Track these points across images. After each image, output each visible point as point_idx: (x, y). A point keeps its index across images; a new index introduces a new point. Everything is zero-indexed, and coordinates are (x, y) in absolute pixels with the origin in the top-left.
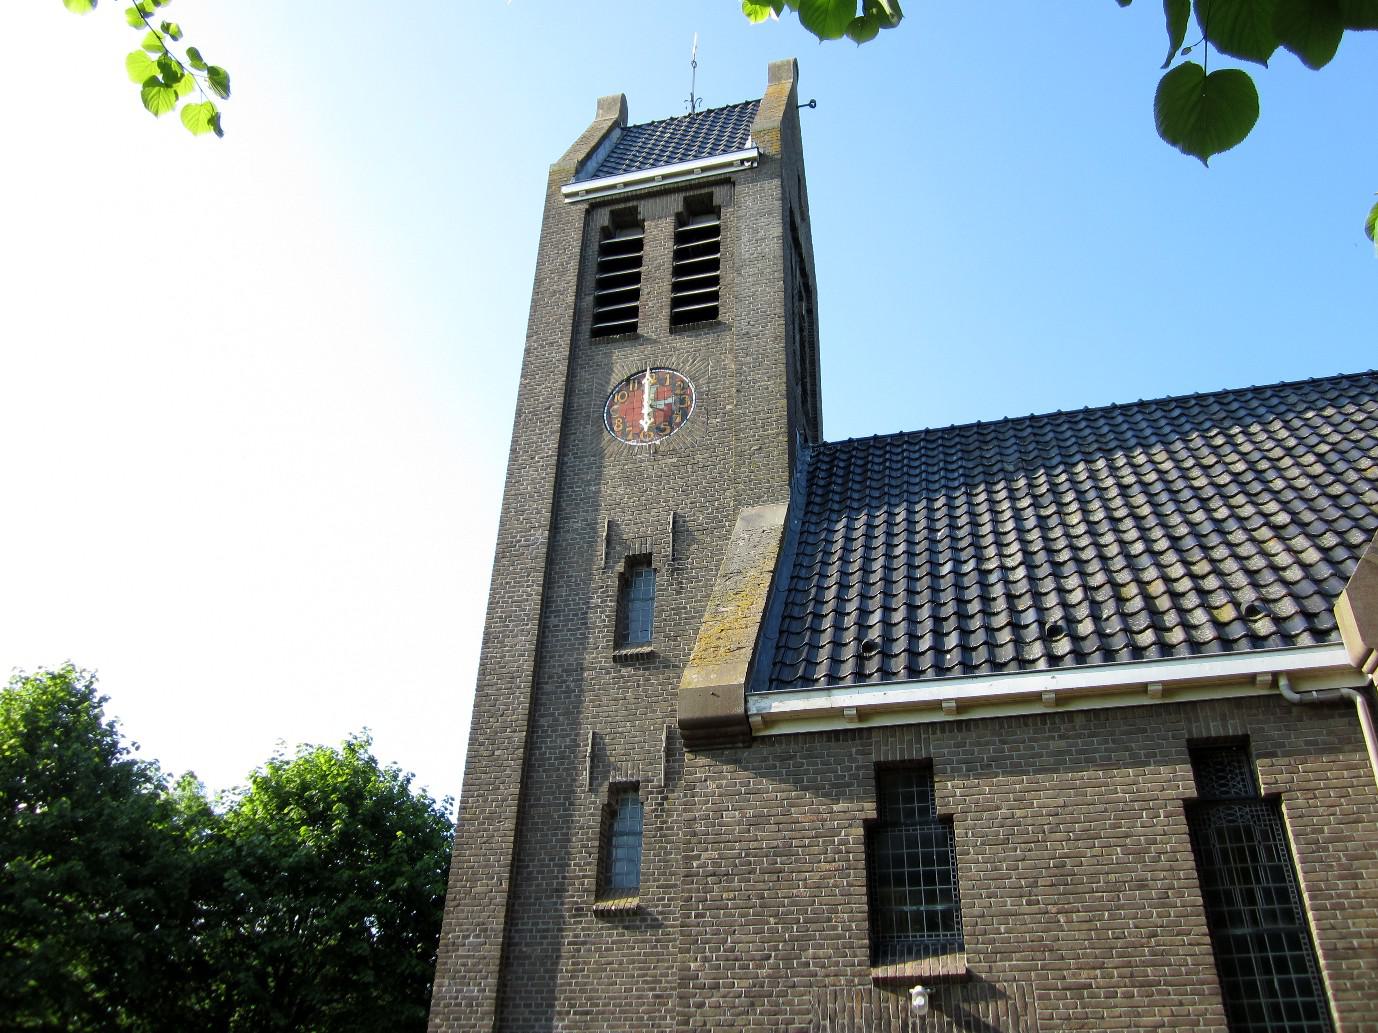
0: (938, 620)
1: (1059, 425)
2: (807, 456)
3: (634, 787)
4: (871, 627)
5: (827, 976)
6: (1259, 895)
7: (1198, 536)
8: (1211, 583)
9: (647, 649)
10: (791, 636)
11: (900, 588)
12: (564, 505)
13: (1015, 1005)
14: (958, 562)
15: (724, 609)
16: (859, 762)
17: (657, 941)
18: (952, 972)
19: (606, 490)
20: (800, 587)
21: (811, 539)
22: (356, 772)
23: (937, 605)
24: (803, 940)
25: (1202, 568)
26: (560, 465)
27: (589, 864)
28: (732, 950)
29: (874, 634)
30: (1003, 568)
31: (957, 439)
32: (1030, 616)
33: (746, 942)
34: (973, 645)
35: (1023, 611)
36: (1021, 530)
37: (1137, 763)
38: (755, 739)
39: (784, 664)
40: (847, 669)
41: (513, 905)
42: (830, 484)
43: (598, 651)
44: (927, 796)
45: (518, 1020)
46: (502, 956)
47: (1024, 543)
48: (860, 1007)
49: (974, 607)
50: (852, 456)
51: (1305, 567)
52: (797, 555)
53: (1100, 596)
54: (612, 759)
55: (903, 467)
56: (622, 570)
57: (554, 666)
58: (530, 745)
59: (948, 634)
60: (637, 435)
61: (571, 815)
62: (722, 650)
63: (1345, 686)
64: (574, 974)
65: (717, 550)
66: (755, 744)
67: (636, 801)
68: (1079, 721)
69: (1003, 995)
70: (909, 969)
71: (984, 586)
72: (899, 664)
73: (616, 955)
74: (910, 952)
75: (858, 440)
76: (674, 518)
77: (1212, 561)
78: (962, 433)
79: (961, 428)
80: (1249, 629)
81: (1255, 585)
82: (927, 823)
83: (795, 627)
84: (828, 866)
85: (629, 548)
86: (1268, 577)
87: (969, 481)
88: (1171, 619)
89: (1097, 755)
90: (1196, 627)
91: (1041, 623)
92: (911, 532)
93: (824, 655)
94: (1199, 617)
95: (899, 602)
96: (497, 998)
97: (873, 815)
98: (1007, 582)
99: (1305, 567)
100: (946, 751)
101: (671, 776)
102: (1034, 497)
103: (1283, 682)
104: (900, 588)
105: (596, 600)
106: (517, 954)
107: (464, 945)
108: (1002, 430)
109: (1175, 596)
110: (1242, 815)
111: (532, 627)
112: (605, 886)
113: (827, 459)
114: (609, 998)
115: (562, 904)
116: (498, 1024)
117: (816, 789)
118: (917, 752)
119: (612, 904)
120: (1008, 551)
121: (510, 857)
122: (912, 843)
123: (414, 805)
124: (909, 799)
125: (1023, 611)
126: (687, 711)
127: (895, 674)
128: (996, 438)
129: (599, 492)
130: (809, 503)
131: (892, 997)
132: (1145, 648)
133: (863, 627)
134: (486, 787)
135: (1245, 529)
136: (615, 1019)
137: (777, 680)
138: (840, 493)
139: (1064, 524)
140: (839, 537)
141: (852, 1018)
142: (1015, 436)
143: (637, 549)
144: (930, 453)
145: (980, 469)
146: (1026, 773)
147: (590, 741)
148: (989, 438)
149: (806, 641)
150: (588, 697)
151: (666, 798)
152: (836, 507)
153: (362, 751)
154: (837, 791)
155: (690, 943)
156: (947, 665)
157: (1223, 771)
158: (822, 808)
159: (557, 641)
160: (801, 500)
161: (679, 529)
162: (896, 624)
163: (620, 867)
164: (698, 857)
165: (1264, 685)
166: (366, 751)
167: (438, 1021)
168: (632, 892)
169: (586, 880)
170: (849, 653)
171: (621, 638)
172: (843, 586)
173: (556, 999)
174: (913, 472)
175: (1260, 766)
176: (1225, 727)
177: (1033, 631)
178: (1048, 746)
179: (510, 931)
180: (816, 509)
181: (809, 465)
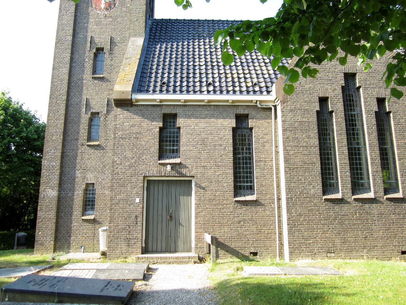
0: (182, 78)
1: (220, 24)
2: (150, 22)
3: (98, 113)
4: (165, 78)
5: (148, 162)
6: (245, 149)
7: (247, 63)
8: (248, 76)
9: (102, 76)
10: (144, 78)
11: (168, 53)
12: (77, 29)
13: (190, 170)
14: (188, 62)
15: (126, 69)
16: (160, 112)
17: (104, 153)
18: (177, 162)
19: (90, 26)
20: (146, 64)
21: (150, 50)
22: (5, 101)
23: (182, 73)
24: (143, 154)
25: (247, 72)
26: (76, 16)
27: (85, 133)
28: (125, 156)
29: (165, 80)
30: (199, 65)
31: (192, 24)
32: (204, 80)
33: (129, 154)
34: (190, 86)
35: (203, 78)
36: (205, 55)
37: (224, 118)
38: (133, 105)
39: (141, 86)
40: (158, 89)
41: (64, 142)
42: (156, 33)
43: (88, 75)
44: (174, 122)
45: (66, 171)
46: (61, 155)
47: (205, 58)
48: (155, 169)
49: (191, 75)
50: (163, 25)
51: (269, 74)
52: (146, 54)
53: (222, 76)
54: (92, 105)
55: (176, 30)
56: (95, 52)
57: (74, 79)
58: (68, 100)
59: (184, 82)
60: (100, 10)
61: (80, 120)
62: (125, 81)
63: (271, 105)
64: (82, 159)
65: (123, 49)
66: (133, 106)
67: (98, 117)
68: (212, 107)
69: (188, 167)
70: (167, 161)
71: (194, 70)
72: (171, 89)
73: (92, 156)
74: (168, 157)
75: (165, 19)
76: (111, 38)
77: (249, 70)
78: (194, 22)
79: (194, 20)
80: (254, 89)
81: (258, 78)
82: (174, 129)
83: (145, 75)
84: (150, 137)
85: (97, 45)
86: (261, 76)
87: (194, 38)
88: (237, 84)
89: (215, 115)
90: (242, 87)
91: (207, 82)
92: (177, 51)
93: (152, 84)
94: (243, 84)
95: (172, 71)
96: (60, 166)
97: (162, 126)
98: (200, 69)
99: (269, 74)
100: (180, 112)
101: (108, 112)
102: (210, 45)
103: (258, 103)
104: (173, 68)
105: (87, 60)
106: (65, 155)
107: (50, 152)
108: (205, 23)
109: (239, 78)
110: (245, 131)
111: (68, 66)
112: (89, 139)
113: (155, 24)
114: (91, 166)
115: (78, 143)
116: (61, 172)
117: (148, 119)
118: (174, 112)
119: (92, 143)
120: (201, 60)
121: (63, 130)
122: (170, 133)
123: (25, 112)
124: (170, 122)
125: (203, 78)
126: (114, 96)
127: (170, 91)
128: (203, 25)
129: (87, 26)
130: (150, 38)
131: (163, 167)
132: (230, 91)
133: (162, 78)
134: (55, 111)
135: (258, 62)
136: (92, 171)
137: (139, 90)
138: (159, 36)
139: (216, 54)
140: (157, 50)
141: (153, 172)
142: (208, 26)
143: (99, 46)
144: (184, 27)
145: (197, 35)
146: (199, 118)
147: (85, 100)
148: (201, 25)
149: (147, 80)
150: (85, 88)
151: (107, 117)
152: (157, 40)
153: (7, 95)
154: (153, 120)
155: (115, 154)
156: (183, 90)
157: (242, 121)
158: (149, 123)
159: (75, 71)
160: (148, 37)
161: (112, 42)
162: (166, 65)
163: (93, 134)
164: (117, 133)
165: (254, 103)
166: (8, 95)
167: (44, 171)
168: (97, 140)
169: (84, 137)
170: (159, 84)
171: (94, 72)
172: (158, 65)
173: (76, 166)
174: (179, 32)
175: (250, 121)
176: (244, 111)
177: (204, 84)
178: (204, 113)
179: (63, 149)
180: (152, 40)
181: (150, 25)
